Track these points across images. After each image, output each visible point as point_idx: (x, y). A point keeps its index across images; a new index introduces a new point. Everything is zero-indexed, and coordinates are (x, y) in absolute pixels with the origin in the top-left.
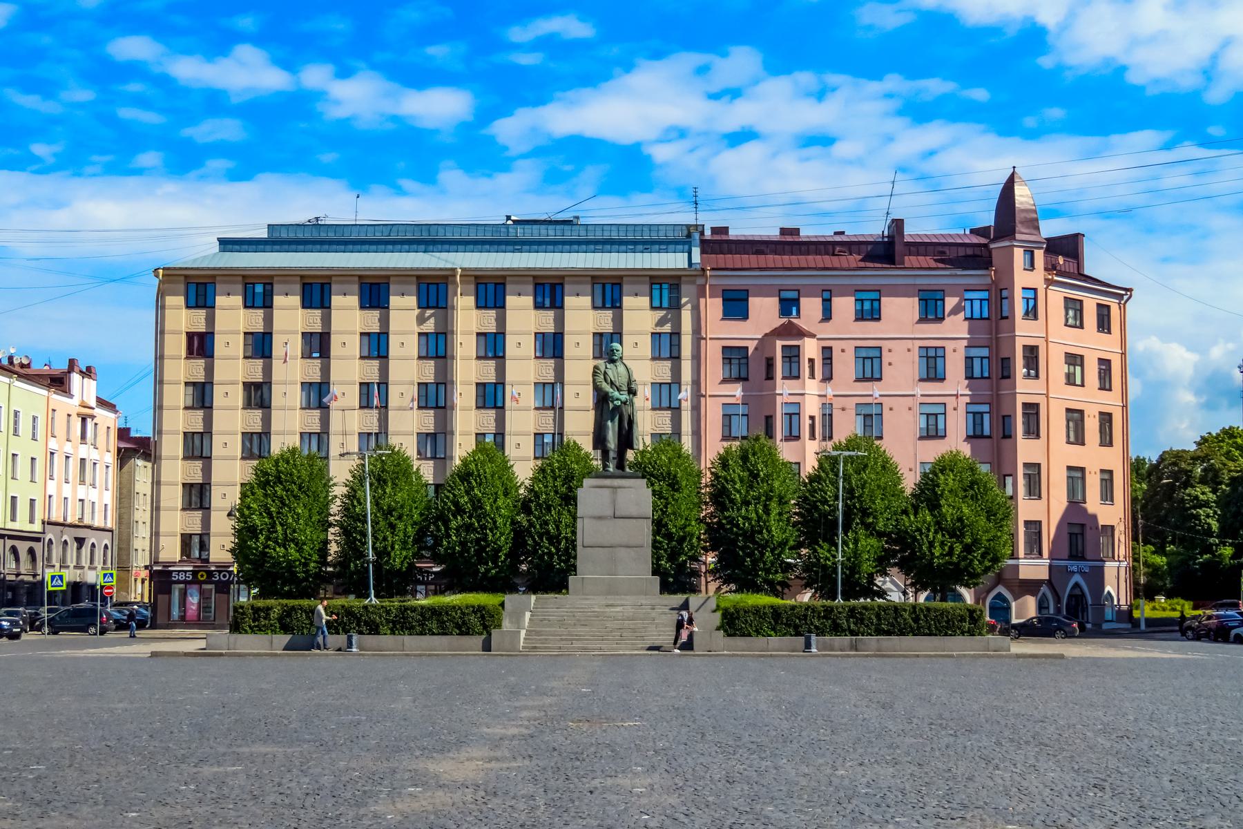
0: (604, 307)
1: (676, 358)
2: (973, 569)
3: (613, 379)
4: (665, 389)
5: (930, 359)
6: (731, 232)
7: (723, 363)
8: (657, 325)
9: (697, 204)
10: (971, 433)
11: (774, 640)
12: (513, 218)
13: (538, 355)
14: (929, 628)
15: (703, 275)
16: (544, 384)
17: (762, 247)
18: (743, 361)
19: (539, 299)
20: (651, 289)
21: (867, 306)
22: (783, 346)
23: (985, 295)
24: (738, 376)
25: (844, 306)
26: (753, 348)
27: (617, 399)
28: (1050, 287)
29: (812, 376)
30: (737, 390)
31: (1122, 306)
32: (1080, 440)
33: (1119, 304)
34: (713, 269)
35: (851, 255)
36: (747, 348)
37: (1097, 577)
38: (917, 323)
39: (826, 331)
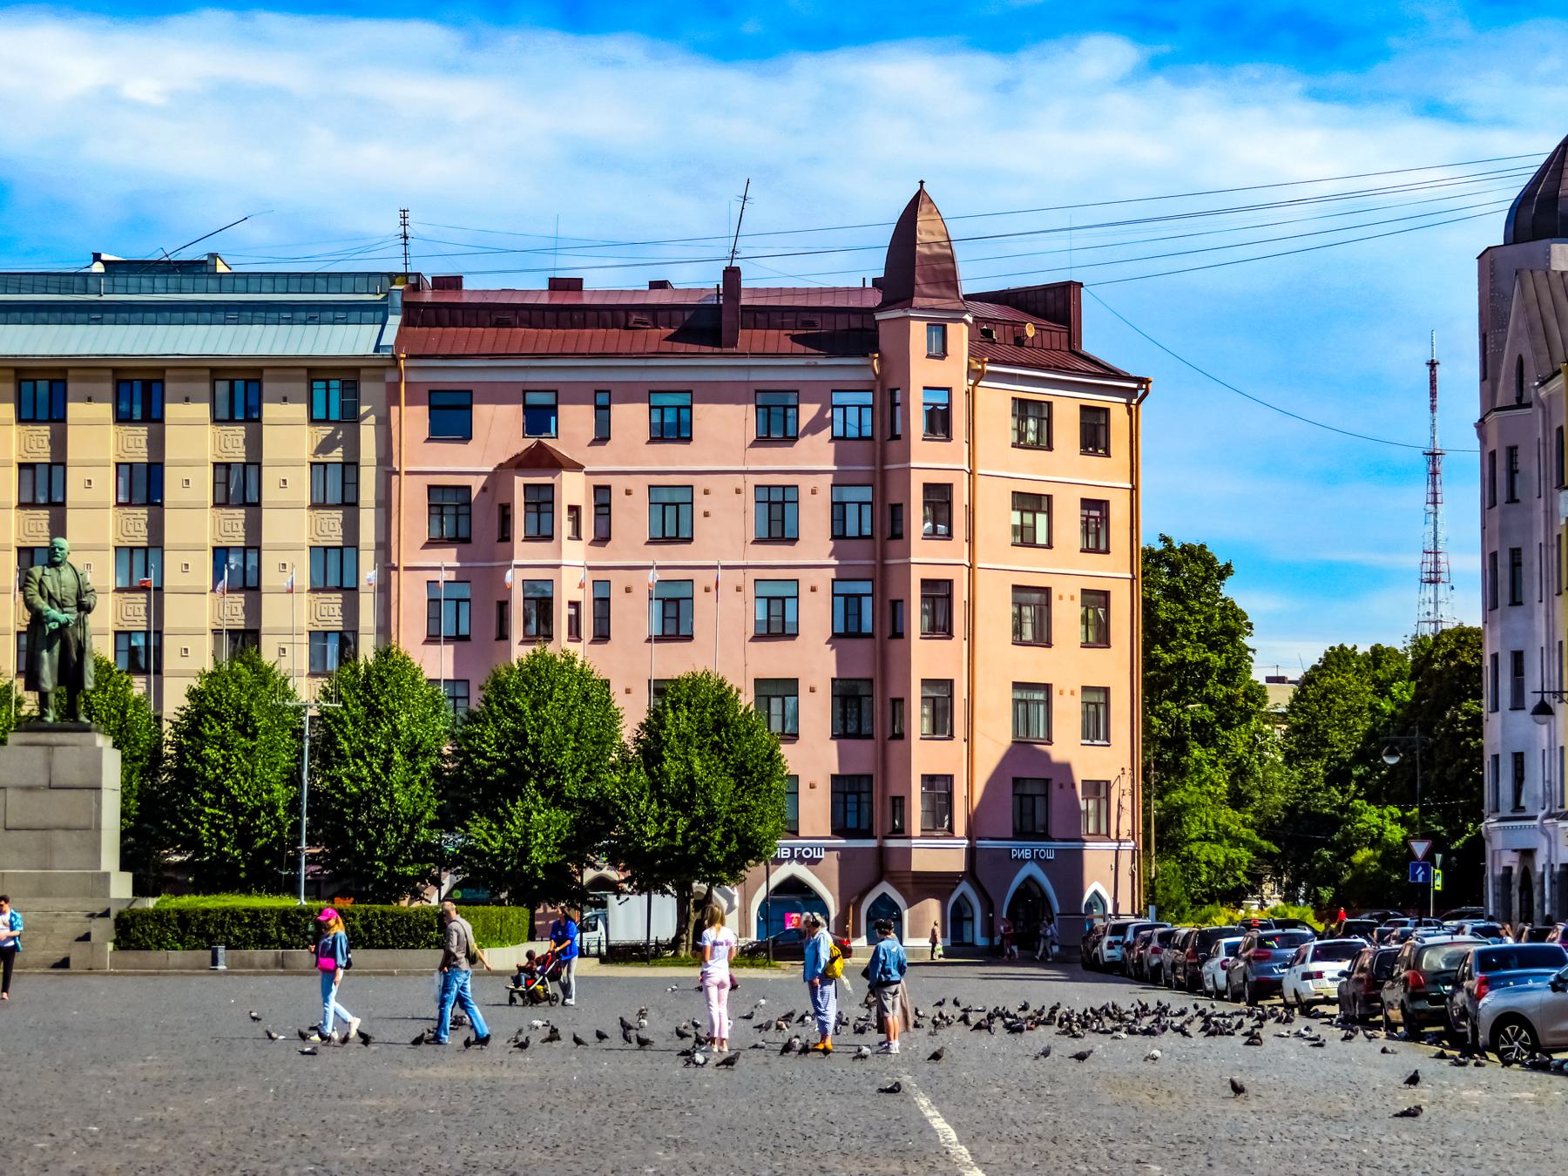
0: (231, 420)
1: (350, 505)
2: (711, 857)
4: (333, 557)
5: (773, 506)
6: (468, 285)
7: (430, 514)
9: (406, 237)
10: (840, 629)
11: (177, 956)
12: (104, 257)
13: (121, 499)
14: (384, 939)
16: (132, 549)
17: (507, 316)
18: (463, 510)
19: (124, 407)
20: (311, 390)
21: (670, 417)
22: (526, 486)
23: (867, 398)
24: (453, 536)
25: (631, 418)
27: (54, 620)
28: (981, 383)
29: (577, 534)
30: (448, 557)
31: (1133, 407)
32: (1043, 638)
33: (1128, 405)
34: (410, 357)
35: (657, 327)
36: (469, 488)
37: (1070, 869)
38: (752, 446)
39: (600, 459)
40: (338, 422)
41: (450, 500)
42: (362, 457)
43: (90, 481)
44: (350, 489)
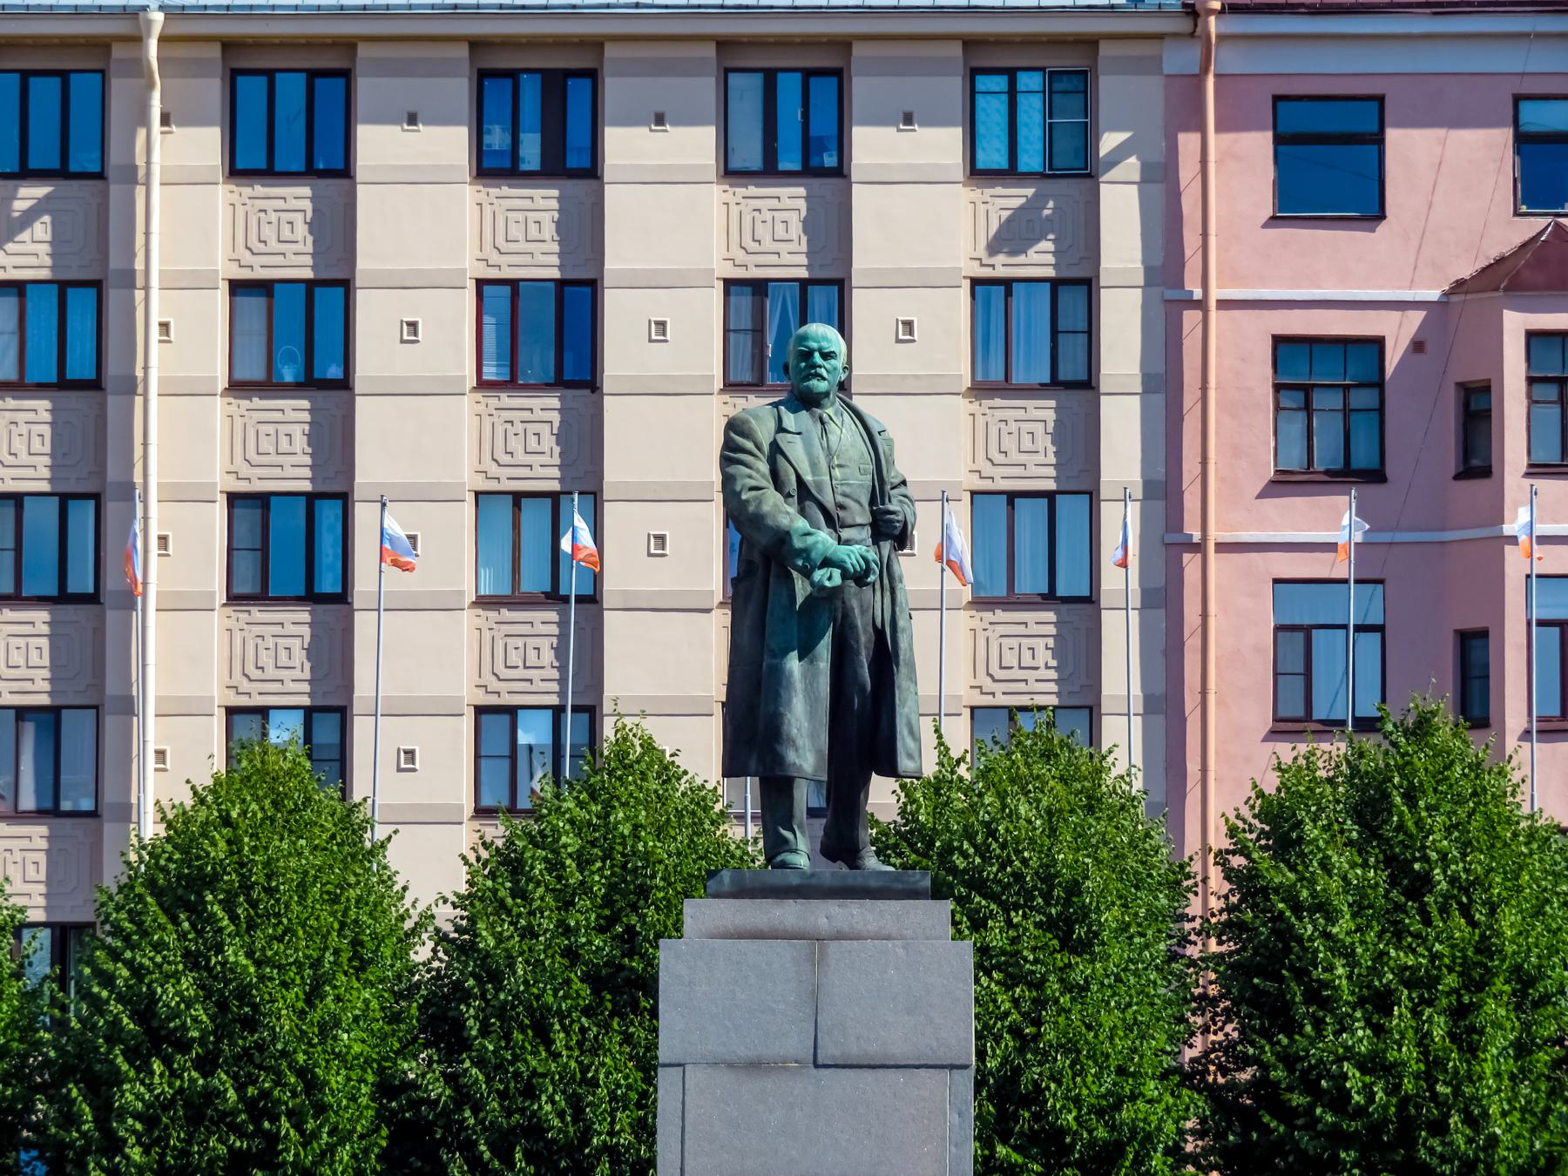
0: (769, 171)
3: (808, 478)
4: (1031, 517)
7: (1278, 408)
8: (994, 248)
13: (490, 373)
15: (1192, 35)
16: (518, 497)
19: (497, 138)
22: (1531, 335)
26: (1404, 343)
27: (827, 563)
34: (1230, 9)
36: (1378, 343)
40: (1043, 176)
41: (1327, 372)
42: (1105, 263)
43: (413, 326)
44: (1072, 348)
